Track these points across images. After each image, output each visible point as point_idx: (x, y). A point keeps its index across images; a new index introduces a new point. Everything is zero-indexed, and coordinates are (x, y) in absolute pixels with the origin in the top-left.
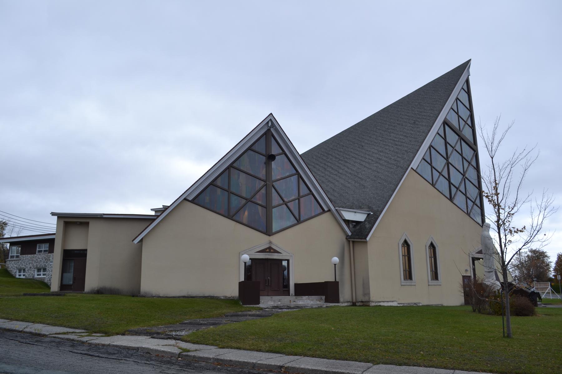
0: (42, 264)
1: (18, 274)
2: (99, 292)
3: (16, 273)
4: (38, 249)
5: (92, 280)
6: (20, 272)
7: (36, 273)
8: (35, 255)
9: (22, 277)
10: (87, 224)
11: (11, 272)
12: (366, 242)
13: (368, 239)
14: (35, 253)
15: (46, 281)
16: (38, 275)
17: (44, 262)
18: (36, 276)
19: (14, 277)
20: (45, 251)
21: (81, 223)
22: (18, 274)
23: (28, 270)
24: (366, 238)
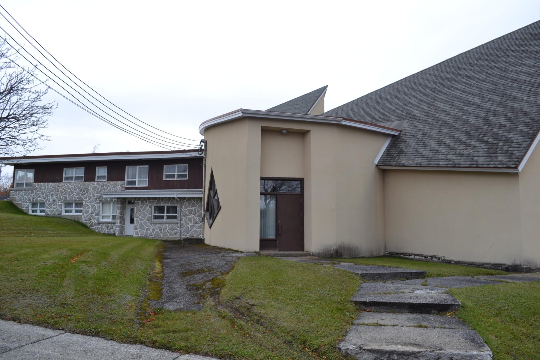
0: (75, 197)
1: (31, 209)
2: (336, 255)
3: (28, 207)
4: (64, 176)
5: (319, 234)
6: (34, 205)
7: (63, 209)
8: (62, 184)
9: (38, 213)
10: (304, 134)
11: (19, 206)
12: (517, 174)
13: (520, 168)
14: (61, 181)
15: (83, 220)
16: (33, 211)
17: (78, 194)
18: (64, 214)
19: (26, 214)
20: (77, 178)
21: (290, 133)
22: (31, 209)
23: (50, 205)
24: (516, 168)
